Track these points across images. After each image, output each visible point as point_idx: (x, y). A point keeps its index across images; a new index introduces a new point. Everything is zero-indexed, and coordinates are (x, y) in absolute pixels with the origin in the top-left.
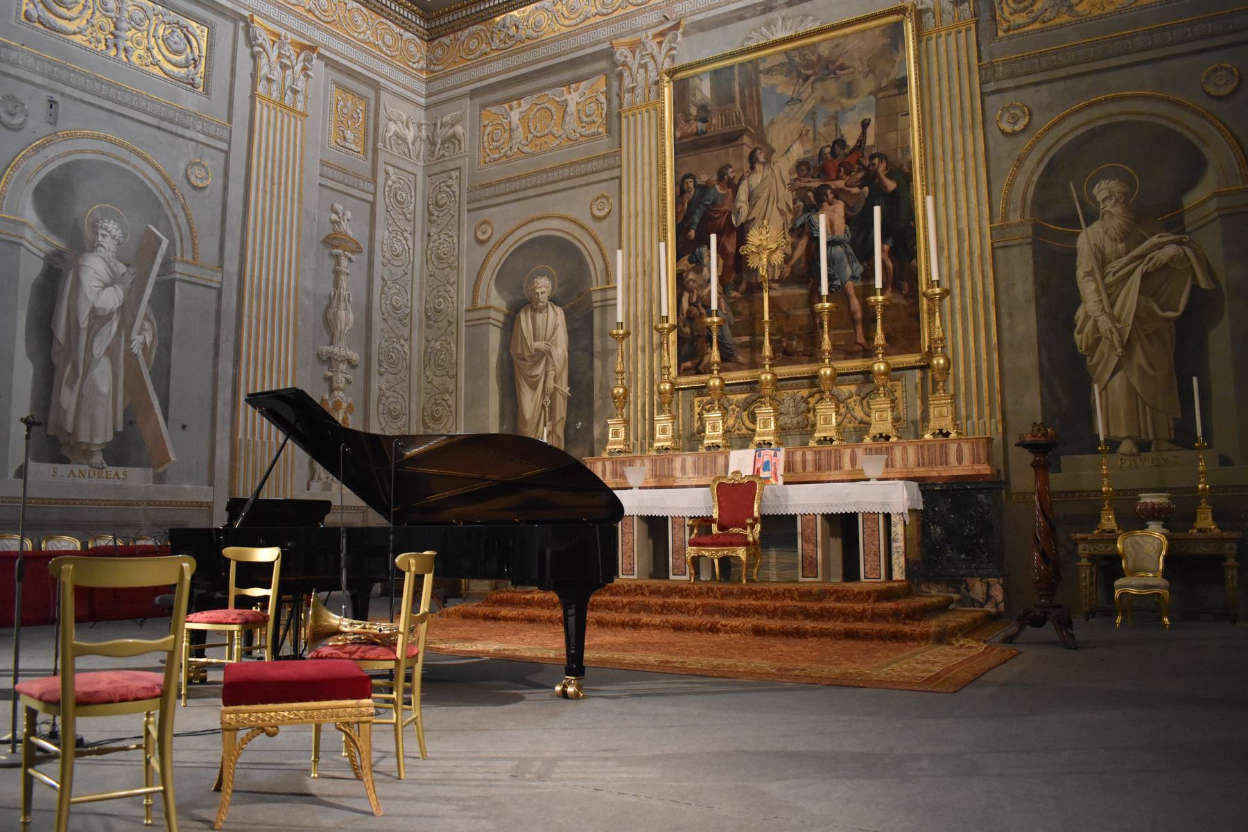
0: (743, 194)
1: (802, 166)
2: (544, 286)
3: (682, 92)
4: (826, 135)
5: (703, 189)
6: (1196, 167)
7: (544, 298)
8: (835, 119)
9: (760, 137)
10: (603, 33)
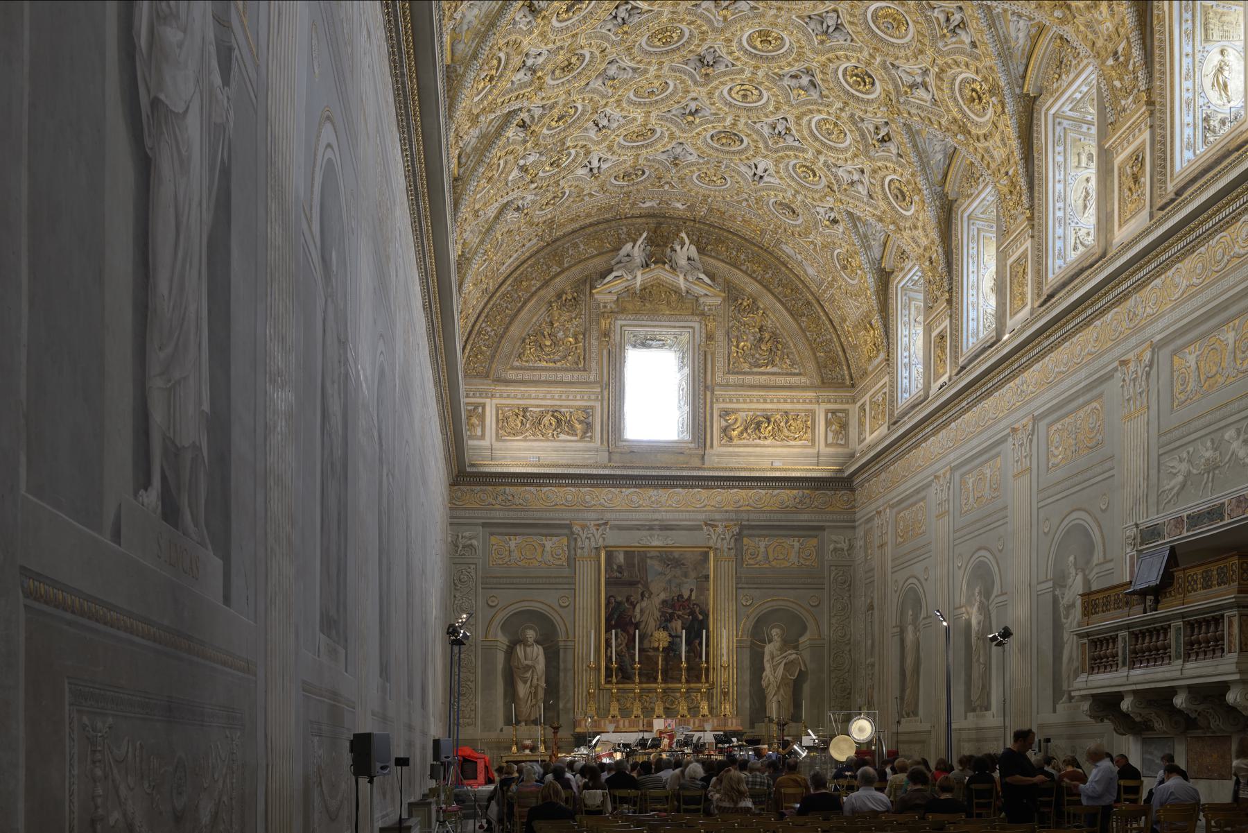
0: (638, 609)
1: (664, 602)
2: (531, 634)
5: (619, 604)
7: (531, 640)
8: (679, 585)
9: (646, 585)
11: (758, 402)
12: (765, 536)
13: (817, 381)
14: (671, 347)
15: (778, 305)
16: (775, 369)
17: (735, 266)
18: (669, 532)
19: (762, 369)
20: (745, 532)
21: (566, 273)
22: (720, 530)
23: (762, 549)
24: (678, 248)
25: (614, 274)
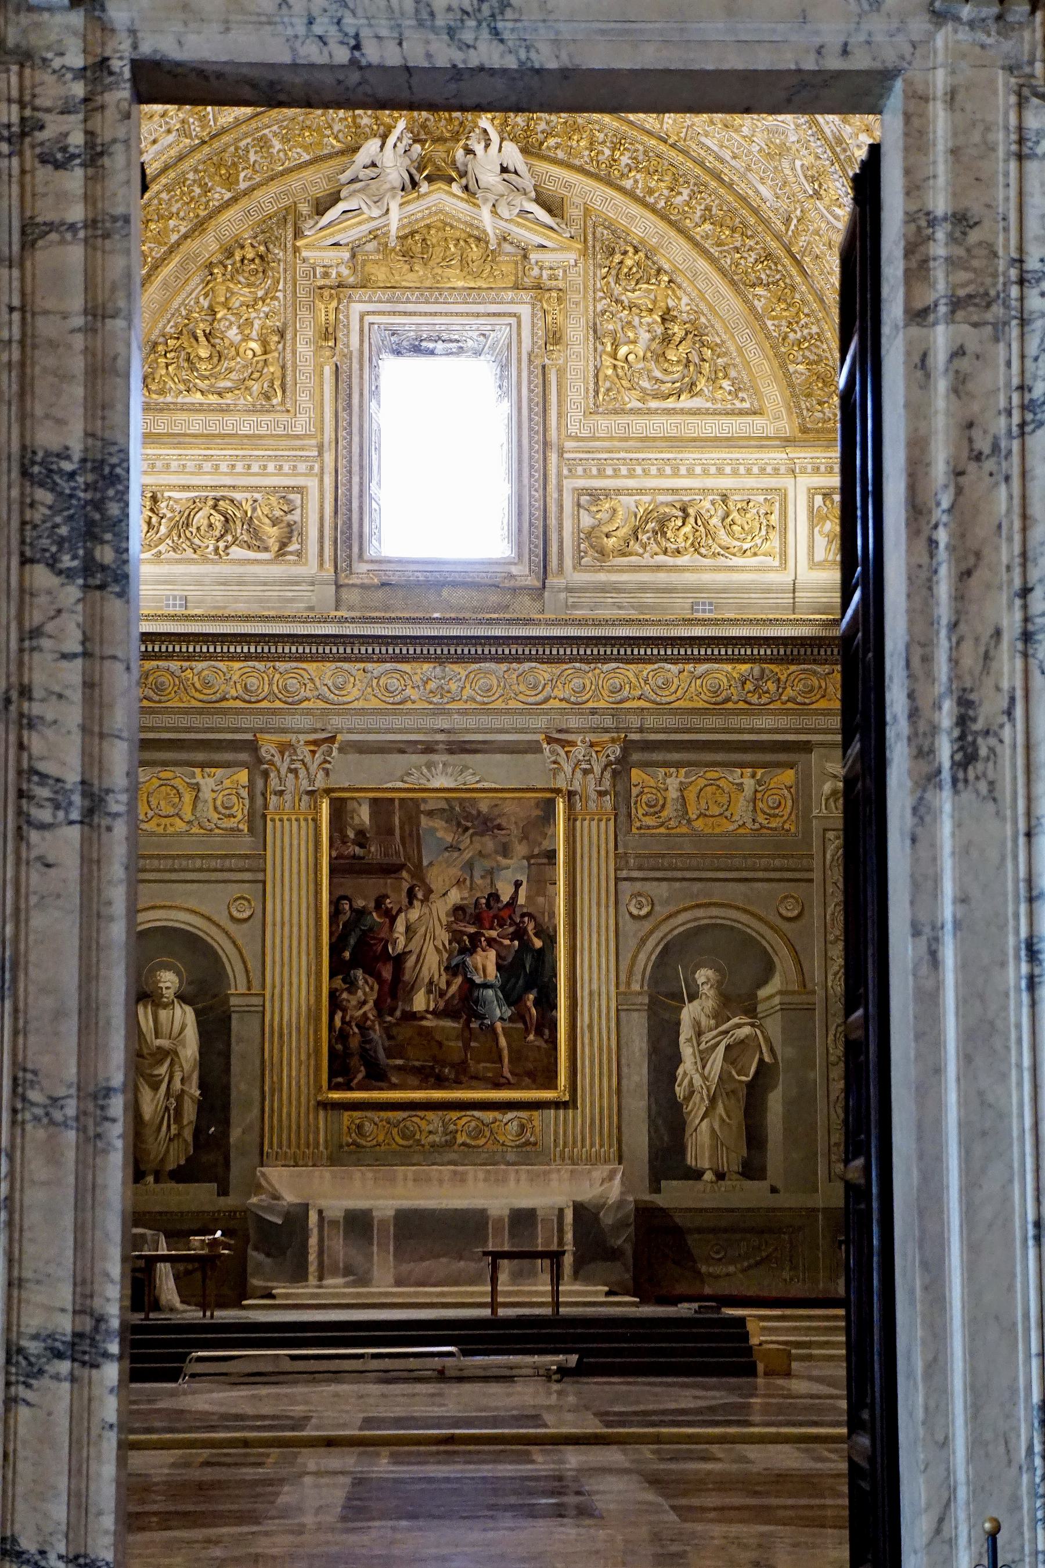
0: (400, 926)
1: (458, 910)
3: (339, 810)
4: (482, 894)
5: (360, 914)
6: (768, 970)
7: (169, 994)
8: (491, 874)
9: (419, 873)
10: (246, 722)
11: (661, 474)
12: (678, 765)
13: (786, 426)
14: (478, 353)
15: (703, 264)
16: (697, 403)
17: (610, 184)
18: (467, 758)
19: (670, 403)
20: (636, 757)
21: (244, 203)
22: (579, 751)
23: (673, 794)
24: (479, 148)
25: (341, 207)
